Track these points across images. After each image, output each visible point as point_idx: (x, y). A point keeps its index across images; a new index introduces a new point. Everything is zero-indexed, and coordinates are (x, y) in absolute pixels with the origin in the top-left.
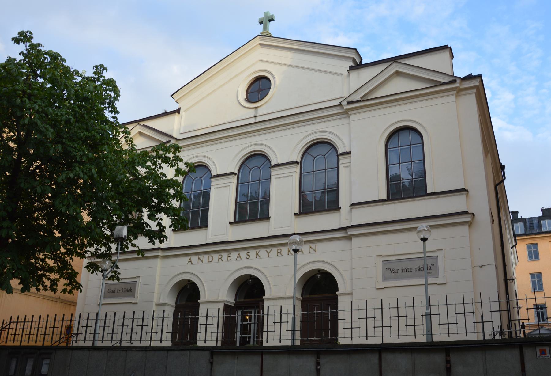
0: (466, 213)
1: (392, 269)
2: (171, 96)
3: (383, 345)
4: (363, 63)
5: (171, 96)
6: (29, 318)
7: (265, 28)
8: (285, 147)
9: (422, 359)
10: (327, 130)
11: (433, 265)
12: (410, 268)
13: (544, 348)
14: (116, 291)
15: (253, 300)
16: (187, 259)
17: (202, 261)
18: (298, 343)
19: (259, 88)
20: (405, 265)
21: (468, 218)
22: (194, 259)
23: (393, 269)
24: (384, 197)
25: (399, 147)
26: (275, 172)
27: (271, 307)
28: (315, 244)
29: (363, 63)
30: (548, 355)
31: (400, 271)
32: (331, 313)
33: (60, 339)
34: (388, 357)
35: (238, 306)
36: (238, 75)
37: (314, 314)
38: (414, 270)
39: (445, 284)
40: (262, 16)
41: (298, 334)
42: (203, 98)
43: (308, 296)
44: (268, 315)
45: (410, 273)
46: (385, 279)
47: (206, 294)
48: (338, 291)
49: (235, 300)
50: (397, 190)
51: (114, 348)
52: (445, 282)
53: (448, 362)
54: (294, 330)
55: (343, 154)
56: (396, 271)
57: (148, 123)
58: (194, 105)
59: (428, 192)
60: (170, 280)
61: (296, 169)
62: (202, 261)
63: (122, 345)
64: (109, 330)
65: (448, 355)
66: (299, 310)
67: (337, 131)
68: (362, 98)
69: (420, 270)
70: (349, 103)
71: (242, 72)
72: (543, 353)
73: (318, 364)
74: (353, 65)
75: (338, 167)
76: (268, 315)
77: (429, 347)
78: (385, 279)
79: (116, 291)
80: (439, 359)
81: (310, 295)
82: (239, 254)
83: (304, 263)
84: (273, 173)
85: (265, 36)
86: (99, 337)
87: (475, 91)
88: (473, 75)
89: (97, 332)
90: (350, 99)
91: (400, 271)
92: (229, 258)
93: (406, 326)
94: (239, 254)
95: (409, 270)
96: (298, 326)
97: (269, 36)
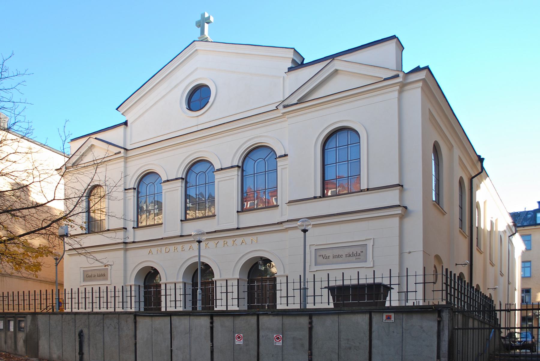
0: (399, 206)
2: (117, 109)
4: (304, 63)
5: (117, 109)
6: (75, 290)
8: (225, 152)
10: (266, 134)
13: (390, 314)
16: (147, 250)
18: (142, 310)
19: (198, 97)
21: (399, 211)
22: (154, 250)
24: (319, 194)
26: (218, 176)
29: (304, 63)
30: (393, 319)
31: (331, 257)
33: (47, 307)
40: (199, 18)
42: (147, 110)
45: (340, 259)
46: (84, 280)
51: (89, 313)
53: (311, 323)
55: (280, 157)
57: (98, 136)
58: (140, 116)
61: (235, 172)
64: (38, 302)
65: (311, 318)
67: (274, 136)
68: (298, 100)
69: (350, 256)
70: (285, 107)
71: (181, 82)
72: (389, 318)
73: (212, 323)
74: (293, 66)
75: (277, 169)
78: (84, 280)
80: (73, 316)
83: (246, 252)
84: (216, 177)
86: (21, 307)
87: (420, 84)
88: (421, 67)
89: (42, 303)
90: (286, 103)
91: (331, 257)
97: (206, 41)
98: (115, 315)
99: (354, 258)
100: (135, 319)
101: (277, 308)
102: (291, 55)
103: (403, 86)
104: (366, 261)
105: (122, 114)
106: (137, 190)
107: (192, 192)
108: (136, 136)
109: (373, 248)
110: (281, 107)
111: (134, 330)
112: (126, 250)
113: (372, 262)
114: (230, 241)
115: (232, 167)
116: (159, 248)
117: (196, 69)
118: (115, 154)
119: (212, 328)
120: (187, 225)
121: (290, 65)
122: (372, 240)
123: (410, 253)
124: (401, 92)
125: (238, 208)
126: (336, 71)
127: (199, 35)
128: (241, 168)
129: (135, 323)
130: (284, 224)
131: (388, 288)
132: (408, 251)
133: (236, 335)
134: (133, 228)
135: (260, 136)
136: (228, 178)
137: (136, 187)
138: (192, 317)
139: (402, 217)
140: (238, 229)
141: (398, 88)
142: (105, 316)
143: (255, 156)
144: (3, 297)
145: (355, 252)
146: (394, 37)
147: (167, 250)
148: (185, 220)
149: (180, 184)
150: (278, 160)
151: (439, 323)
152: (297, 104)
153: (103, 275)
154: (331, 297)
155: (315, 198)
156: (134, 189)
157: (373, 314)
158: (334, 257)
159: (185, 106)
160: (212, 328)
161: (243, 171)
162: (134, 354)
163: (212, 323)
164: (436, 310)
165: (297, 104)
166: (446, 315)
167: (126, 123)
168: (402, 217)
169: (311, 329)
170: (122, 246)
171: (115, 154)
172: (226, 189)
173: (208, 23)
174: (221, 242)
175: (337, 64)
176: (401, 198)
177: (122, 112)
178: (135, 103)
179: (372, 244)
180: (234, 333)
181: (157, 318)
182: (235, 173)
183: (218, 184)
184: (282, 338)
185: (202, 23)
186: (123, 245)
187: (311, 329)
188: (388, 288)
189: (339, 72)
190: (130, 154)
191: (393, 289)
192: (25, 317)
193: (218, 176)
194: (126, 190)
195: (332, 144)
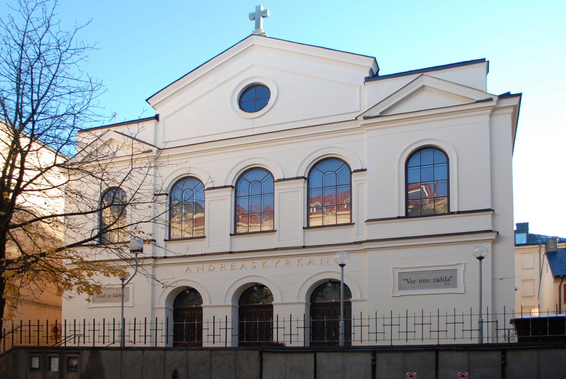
0: (491, 231)
2: (147, 100)
3: (439, 346)
5: (147, 100)
7: (258, 26)
8: (288, 161)
9: (476, 357)
11: (451, 277)
12: (427, 279)
14: (107, 296)
16: (186, 267)
19: (253, 97)
20: (422, 277)
21: (492, 236)
22: (193, 268)
23: (409, 281)
24: (403, 214)
25: (421, 166)
27: (280, 312)
28: (327, 257)
31: (417, 282)
32: (194, 324)
34: (443, 356)
36: (228, 80)
38: (432, 281)
40: (254, 10)
41: (171, 339)
48: (351, 297)
49: (239, 304)
50: (414, 209)
53: (504, 359)
54: (167, 336)
56: (413, 282)
57: (119, 129)
59: (451, 211)
61: (302, 184)
63: (67, 345)
66: (171, 322)
67: (353, 149)
68: (381, 113)
69: (438, 281)
70: (365, 118)
73: (374, 360)
77: (480, 348)
78: (400, 288)
79: (107, 296)
85: (258, 35)
87: (511, 110)
88: (512, 93)
89: (92, 332)
90: (367, 115)
91: (417, 282)
92: (233, 268)
95: (426, 281)
96: (171, 333)
98: (229, 352)
99: (443, 283)
100: (261, 355)
102: (370, 64)
103: (495, 109)
105: (153, 107)
106: (170, 195)
107: (244, 204)
108: (170, 132)
109: (464, 273)
110: (361, 118)
111: (259, 369)
112: (155, 266)
113: (463, 288)
114: (294, 261)
115: (297, 178)
116: (201, 266)
117: (253, 66)
118: (144, 152)
119: (374, 367)
120: (237, 239)
121: (368, 75)
122: (463, 265)
123: (501, 279)
124: (491, 115)
125: (304, 224)
126: (423, 87)
127: (254, 29)
128: (235, 188)
129: (261, 361)
130: (363, 244)
132: (500, 277)
133: (408, 374)
134: (165, 240)
135: (332, 147)
136: (222, 198)
137: (234, 185)
138: (346, 354)
139: (494, 242)
140: (304, 247)
141: (489, 111)
142: (214, 352)
143: (323, 167)
144: (38, 326)
145: (443, 277)
146: (483, 60)
147: (212, 268)
148: (235, 234)
149: (229, 193)
150: (275, 183)
152: (378, 116)
155: (399, 218)
156: (167, 194)
158: (420, 281)
159: (237, 106)
160: (374, 367)
161: (236, 191)
163: (374, 360)
165: (378, 116)
167: (157, 117)
168: (494, 242)
169: (504, 365)
170: (151, 261)
171: (144, 152)
172: (290, 202)
173: (263, 17)
174: (283, 261)
175: (426, 80)
176: (493, 224)
177: (152, 105)
178: (171, 95)
179: (463, 269)
180: (405, 371)
181: (294, 355)
182: (229, 194)
183: (209, 204)
185: (257, 16)
186: (152, 260)
187: (504, 365)
189: (425, 88)
190: (165, 153)
192: (79, 353)
193: (278, 187)
194: (155, 195)
195: (415, 161)
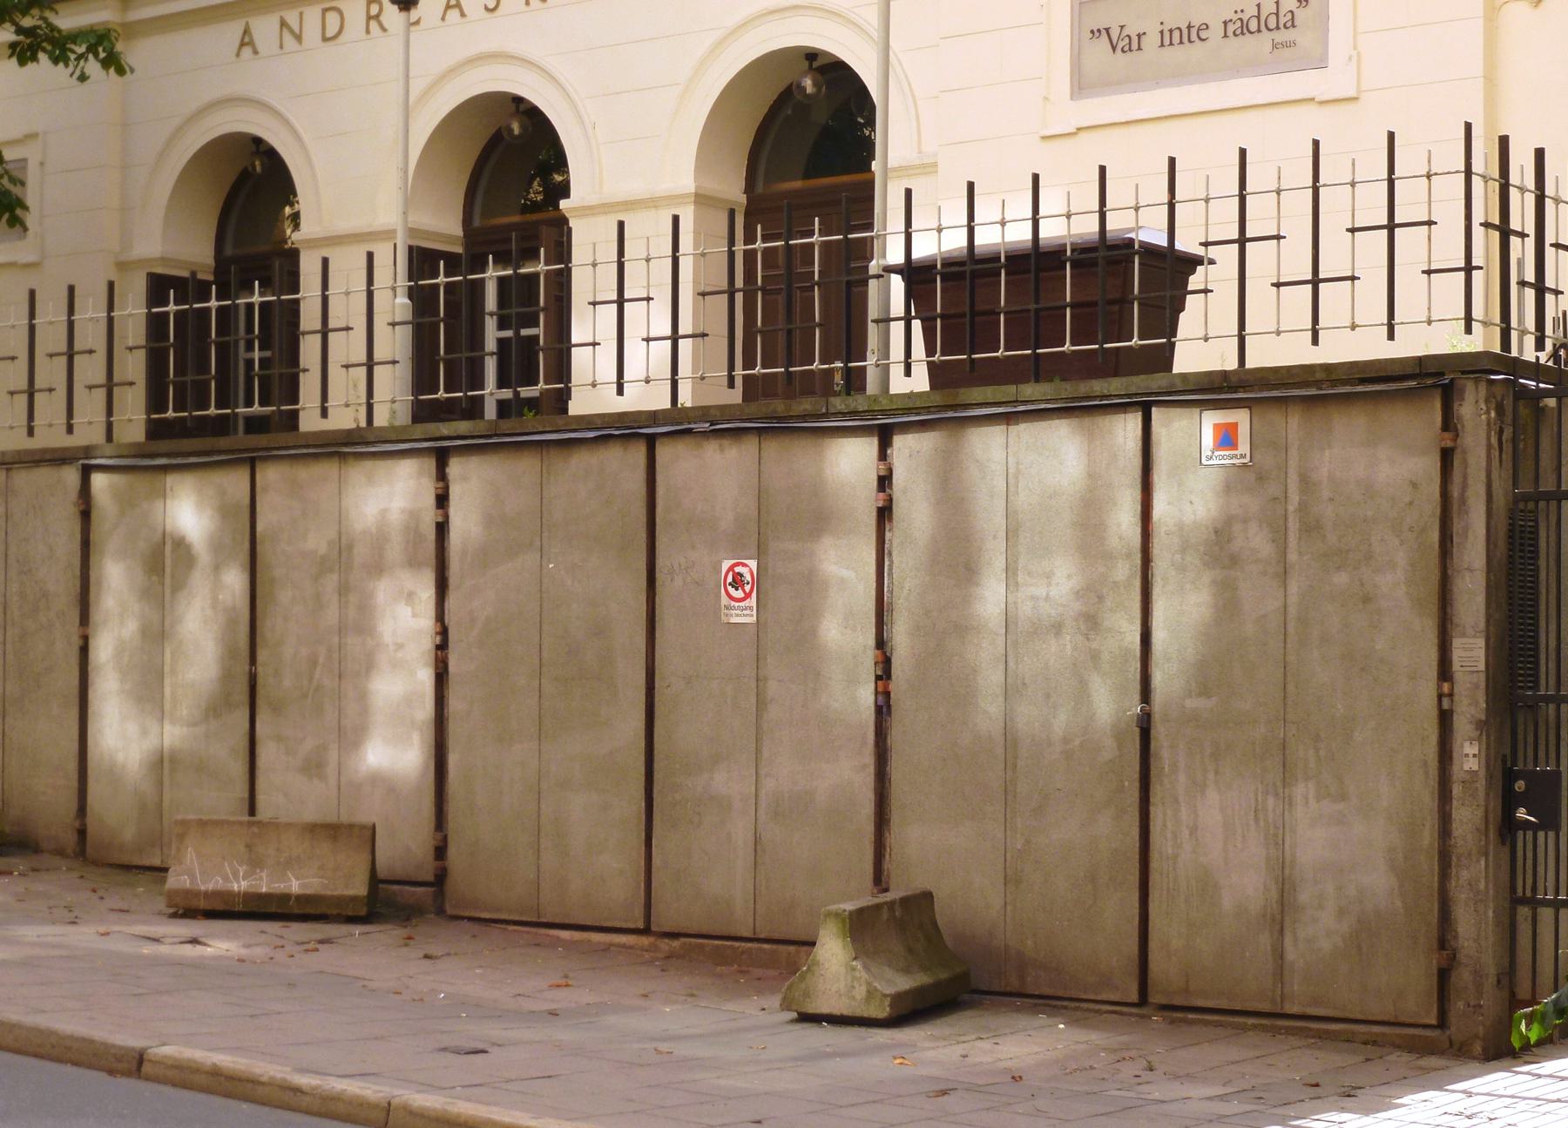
1: (1115, 34)
15: (846, 178)
17: (298, 38)
31: (1151, 41)
32: (177, 313)
35: (482, 243)
37: (208, 310)
39: (1356, 99)
43: (798, 184)
44: (1468, 173)
45: (1196, 51)
46: (1081, 86)
47: (593, 179)
52: (1352, 93)
60: (722, 43)
62: (298, 38)
69: (1244, 29)
76: (1468, 173)
78: (1081, 86)
81: (807, 175)
82: (246, 31)
91: (1151, 41)
93: (648, 299)
94: (246, 31)
95: (1191, 34)
99: (1266, 37)
101: (571, 412)
104: (1321, 64)
131: (1170, 271)
145: (1269, 7)
151: (1447, 456)
153: (1275, 46)
154: (917, 325)
157: (1155, 412)
162: (74, 713)
164: (1433, 379)
166: (1473, 409)
184: (759, 581)
188: (1170, 271)
191: (1212, 262)
